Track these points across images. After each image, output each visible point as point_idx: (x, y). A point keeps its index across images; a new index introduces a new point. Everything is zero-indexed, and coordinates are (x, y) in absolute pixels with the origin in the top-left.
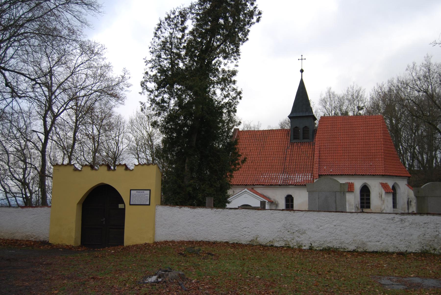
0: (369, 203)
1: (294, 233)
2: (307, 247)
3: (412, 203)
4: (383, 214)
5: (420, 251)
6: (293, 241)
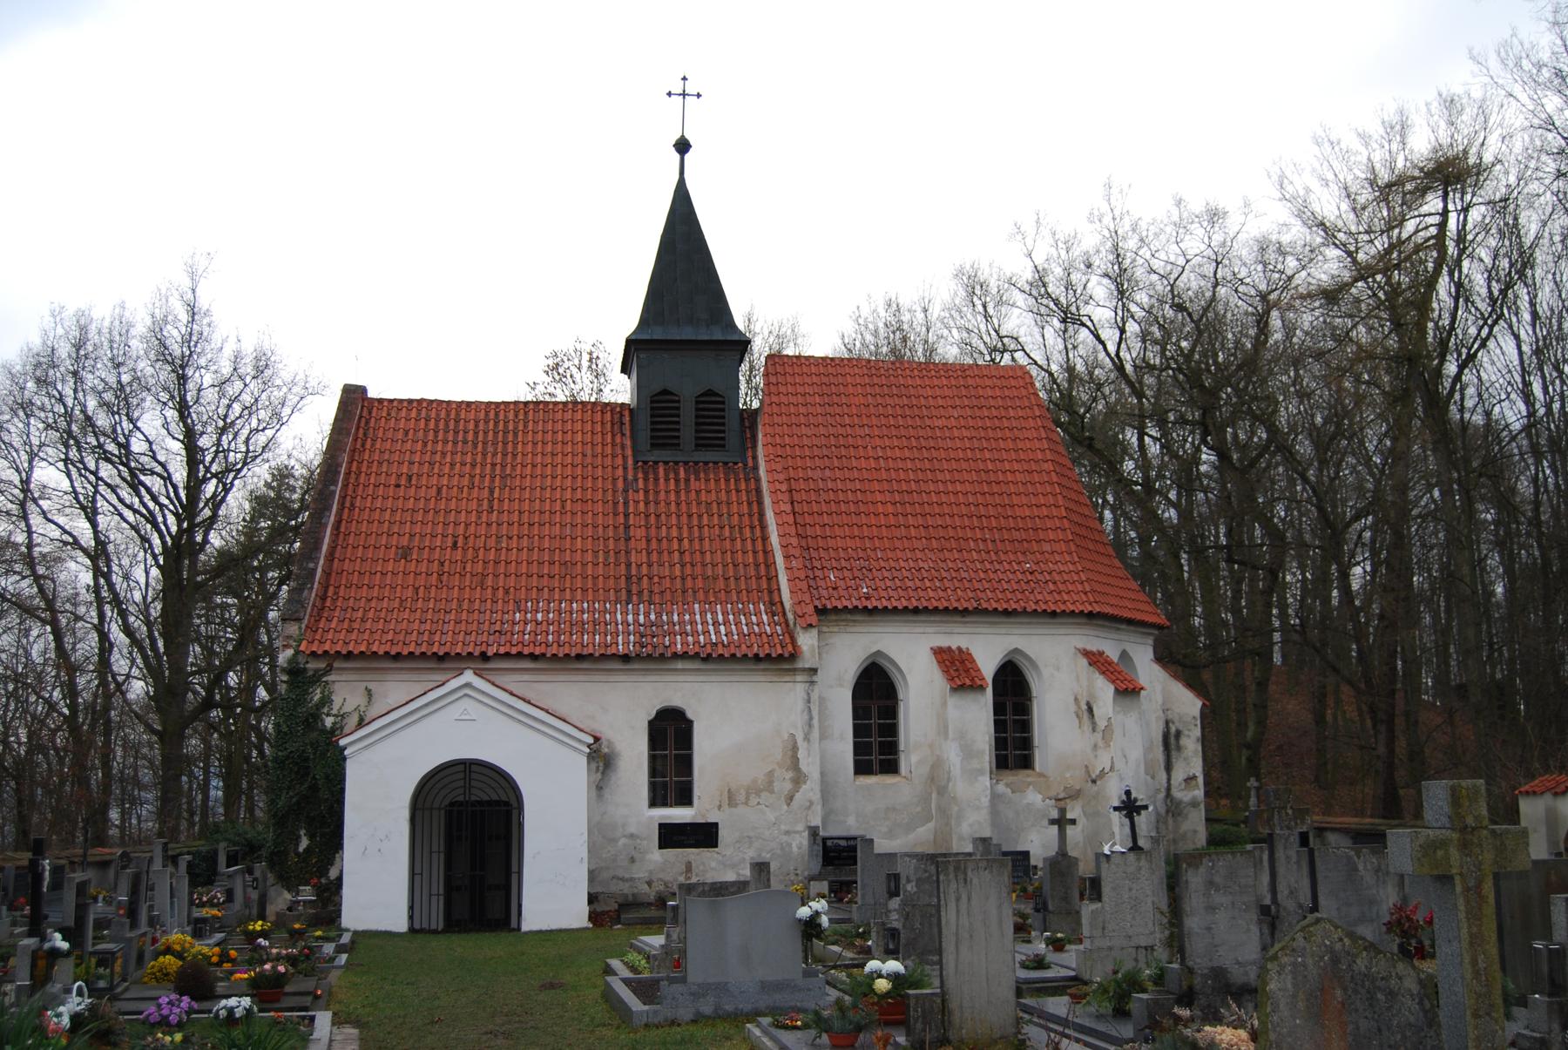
3: (1184, 741)
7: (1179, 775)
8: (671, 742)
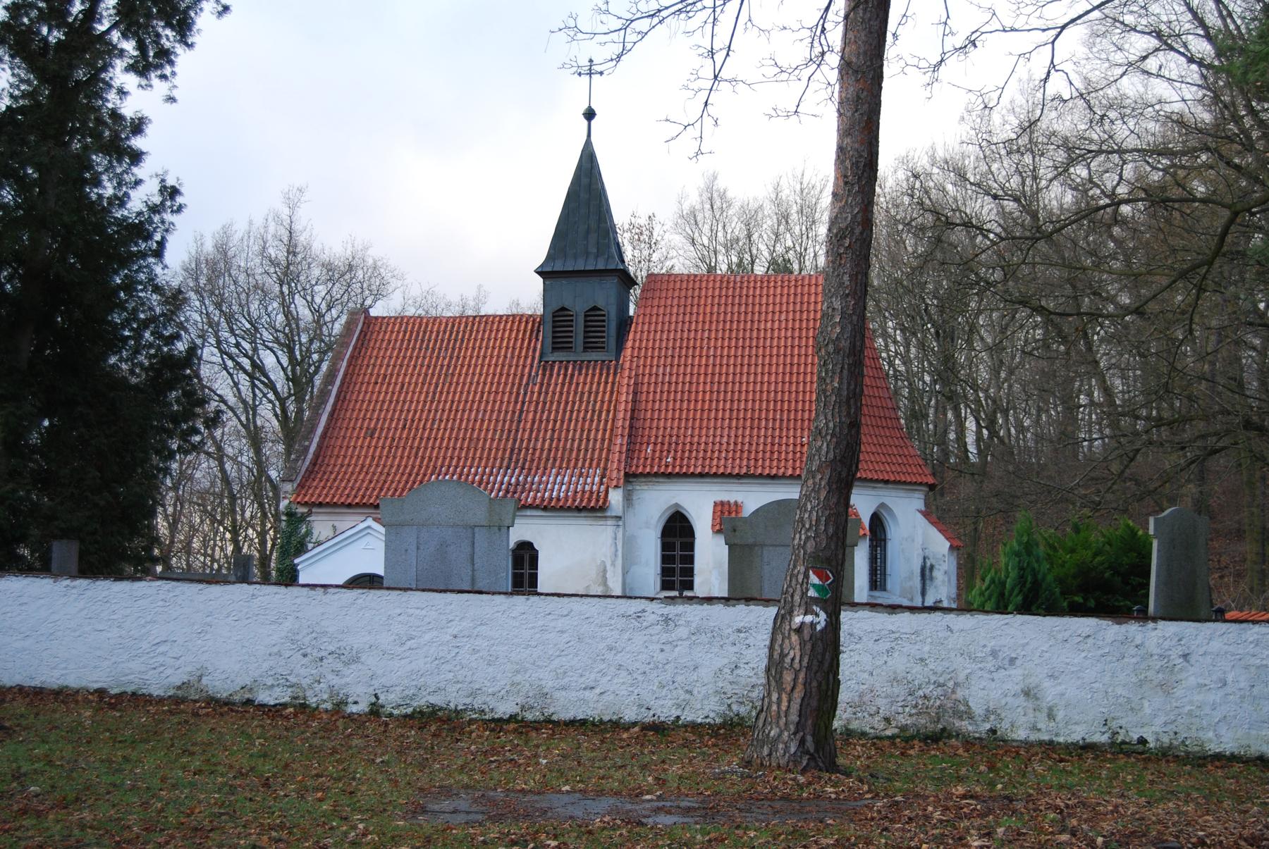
0: (690, 572)
1: (321, 659)
2: (362, 707)
3: (935, 573)
4: (609, 600)
5: (719, 721)
6: (317, 687)
8: (527, 565)
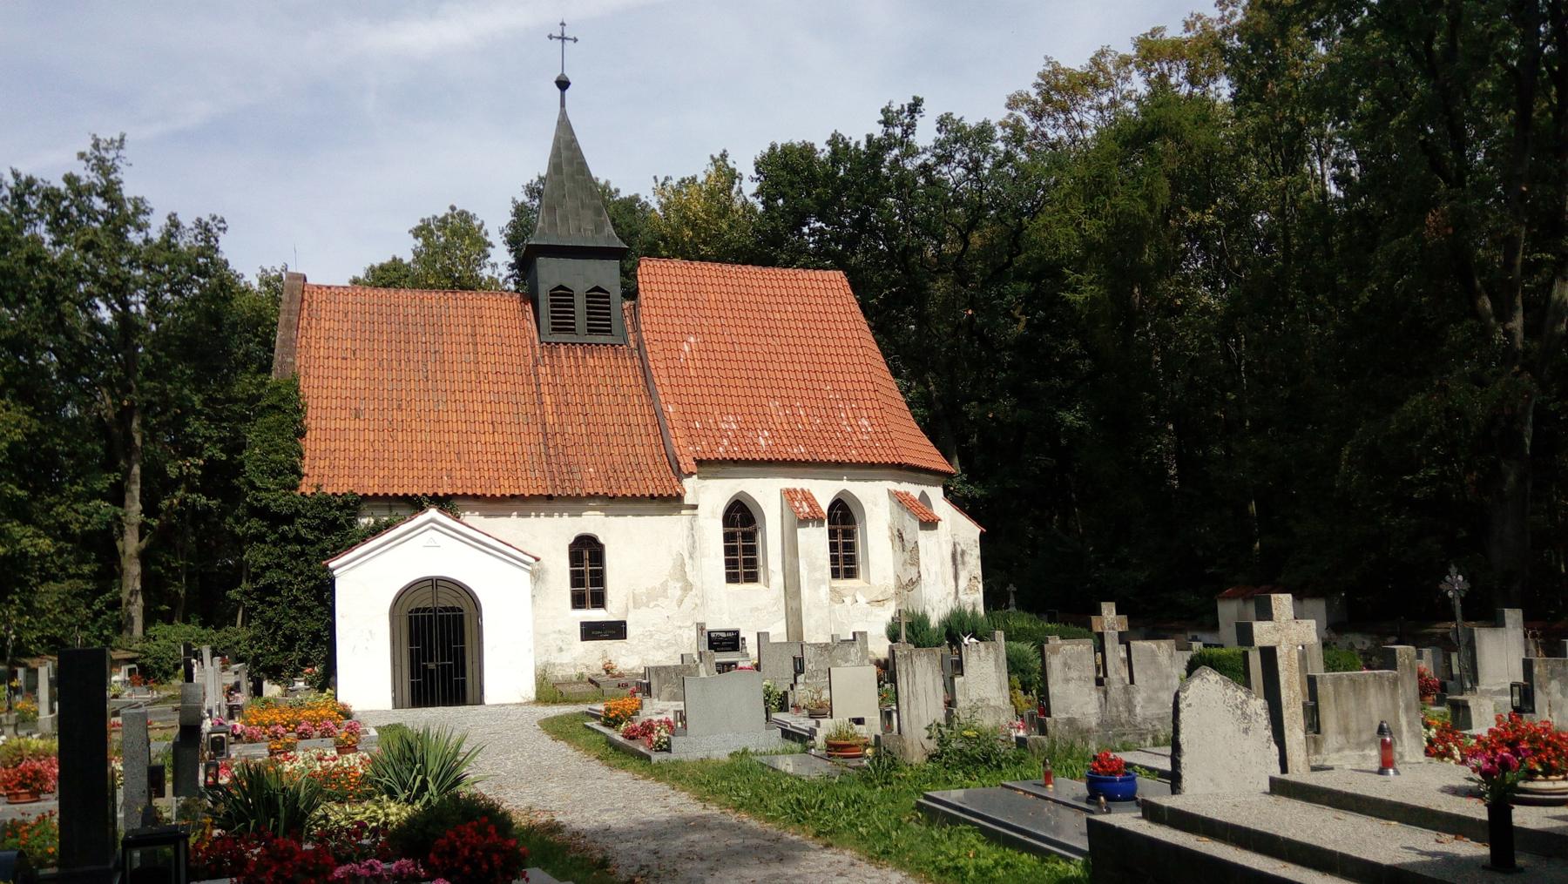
3: (967, 558)
7: (963, 583)
